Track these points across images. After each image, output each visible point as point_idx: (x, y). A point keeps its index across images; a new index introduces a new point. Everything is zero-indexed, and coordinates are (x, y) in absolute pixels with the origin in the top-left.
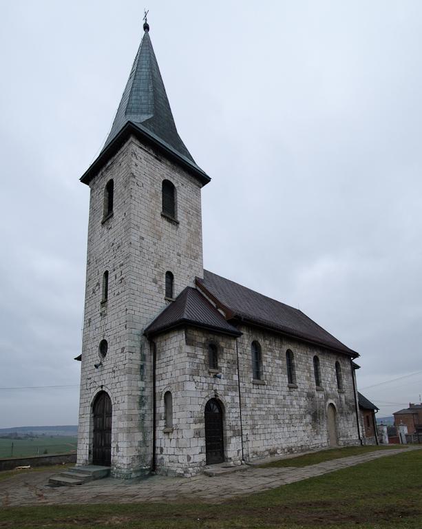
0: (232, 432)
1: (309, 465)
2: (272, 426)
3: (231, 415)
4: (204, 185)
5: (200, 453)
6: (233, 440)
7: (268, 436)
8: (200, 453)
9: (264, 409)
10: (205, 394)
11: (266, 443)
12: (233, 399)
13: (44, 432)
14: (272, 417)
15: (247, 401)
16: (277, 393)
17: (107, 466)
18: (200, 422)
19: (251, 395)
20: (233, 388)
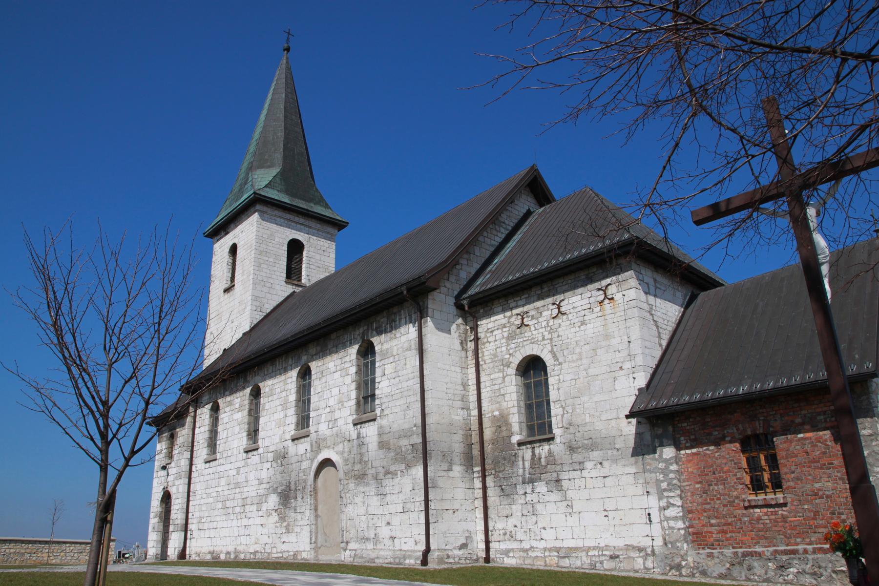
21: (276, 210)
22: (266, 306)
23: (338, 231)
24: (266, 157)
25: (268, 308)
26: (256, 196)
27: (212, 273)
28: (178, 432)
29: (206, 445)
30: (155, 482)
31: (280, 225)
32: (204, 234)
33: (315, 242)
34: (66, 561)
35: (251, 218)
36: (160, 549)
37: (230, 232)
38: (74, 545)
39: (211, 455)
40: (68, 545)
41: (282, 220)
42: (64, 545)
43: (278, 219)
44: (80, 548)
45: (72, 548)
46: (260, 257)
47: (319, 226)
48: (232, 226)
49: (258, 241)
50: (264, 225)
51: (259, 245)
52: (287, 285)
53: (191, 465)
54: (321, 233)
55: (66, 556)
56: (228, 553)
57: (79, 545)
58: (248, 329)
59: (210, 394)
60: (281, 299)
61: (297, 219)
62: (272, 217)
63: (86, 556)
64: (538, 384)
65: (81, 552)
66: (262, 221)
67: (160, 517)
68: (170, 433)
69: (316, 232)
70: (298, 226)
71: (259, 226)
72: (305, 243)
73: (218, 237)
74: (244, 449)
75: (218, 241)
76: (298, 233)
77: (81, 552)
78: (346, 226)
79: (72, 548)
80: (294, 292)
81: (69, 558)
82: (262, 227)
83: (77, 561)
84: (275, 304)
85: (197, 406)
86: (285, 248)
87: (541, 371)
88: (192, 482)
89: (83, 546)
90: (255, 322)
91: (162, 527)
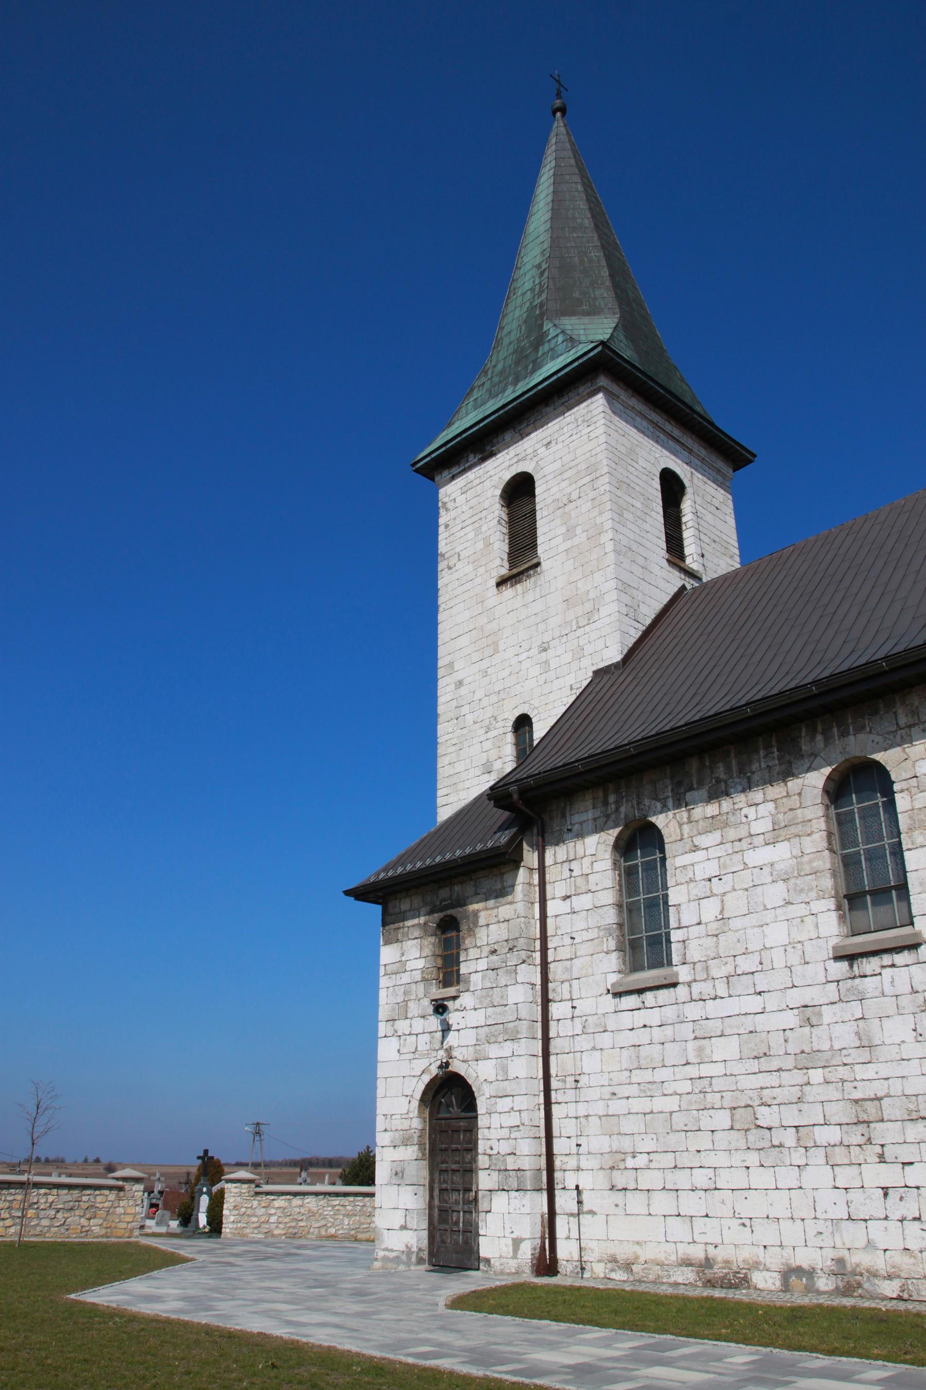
0: (495, 1174)
1: (631, 1329)
2: (721, 1159)
3: (495, 1120)
4: (533, 495)
5: (404, 1228)
6: (500, 1202)
7: (691, 1204)
8: (404, 1228)
9: (669, 1088)
10: (421, 1064)
11: (678, 1229)
12: (505, 1069)
13: (299, 1338)
14: (722, 1119)
15: (590, 1063)
16: (755, 1003)
17: (417, 469)
18: (406, 1142)
19: (605, 1040)
20: (505, 1031)
21: (633, 396)
22: (644, 609)
23: (734, 471)
24: (576, 295)
25: (648, 614)
26: (607, 351)
27: (442, 547)
28: (476, 914)
29: (612, 944)
30: (387, 1050)
31: (643, 433)
32: (413, 465)
33: (700, 484)
34: (39, 1229)
35: (580, 410)
36: (425, 1234)
37: (500, 452)
38: (55, 1191)
39: (627, 974)
40: (42, 1191)
41: (645, 423)
42: (35, 1192)
43: (638, 419)
44: (69, 1198)
45: (51, 1198)
46: (619, 493)
47: (703, 452)
48: (508, 436)
49: (611, 456)
50: (617, 423)
51: (613, 465)
52: (671, 569)
53: (546, 1002)
54: (707, 469)
55: (38, 1217)
56: (789, 1273)
57: (66, 1191)
58: (614, 655)
59: (606, 803)
60: (666, 599)
61: (668, 427)
62: (627, 411)
63: (81, 1217)
64: (649, 867)
65: (71, 1209)
66: (613, 416)
67: (421, 1145)
68: (437, 916)
69: (699, 463)
70: (671, 443)
71: (609, 424)
72: (686, 482)
73: (455, 470)
74: (835, 948)
75: (453, 478)
76: (673, 457)
77: (71, 1209)
78: (751, 462)
79: (51, 1198)
80: (683, 588)
81: (45, 1222)
82: (613, 426)
83: (63, 1231)
84: (658, 607)
85: (544, 841)
86: (657, 480)
87: (656, 848)
88: (552, 1049)
89: (76, 1193)
90: (631, 642)
91: (425, 1173)
